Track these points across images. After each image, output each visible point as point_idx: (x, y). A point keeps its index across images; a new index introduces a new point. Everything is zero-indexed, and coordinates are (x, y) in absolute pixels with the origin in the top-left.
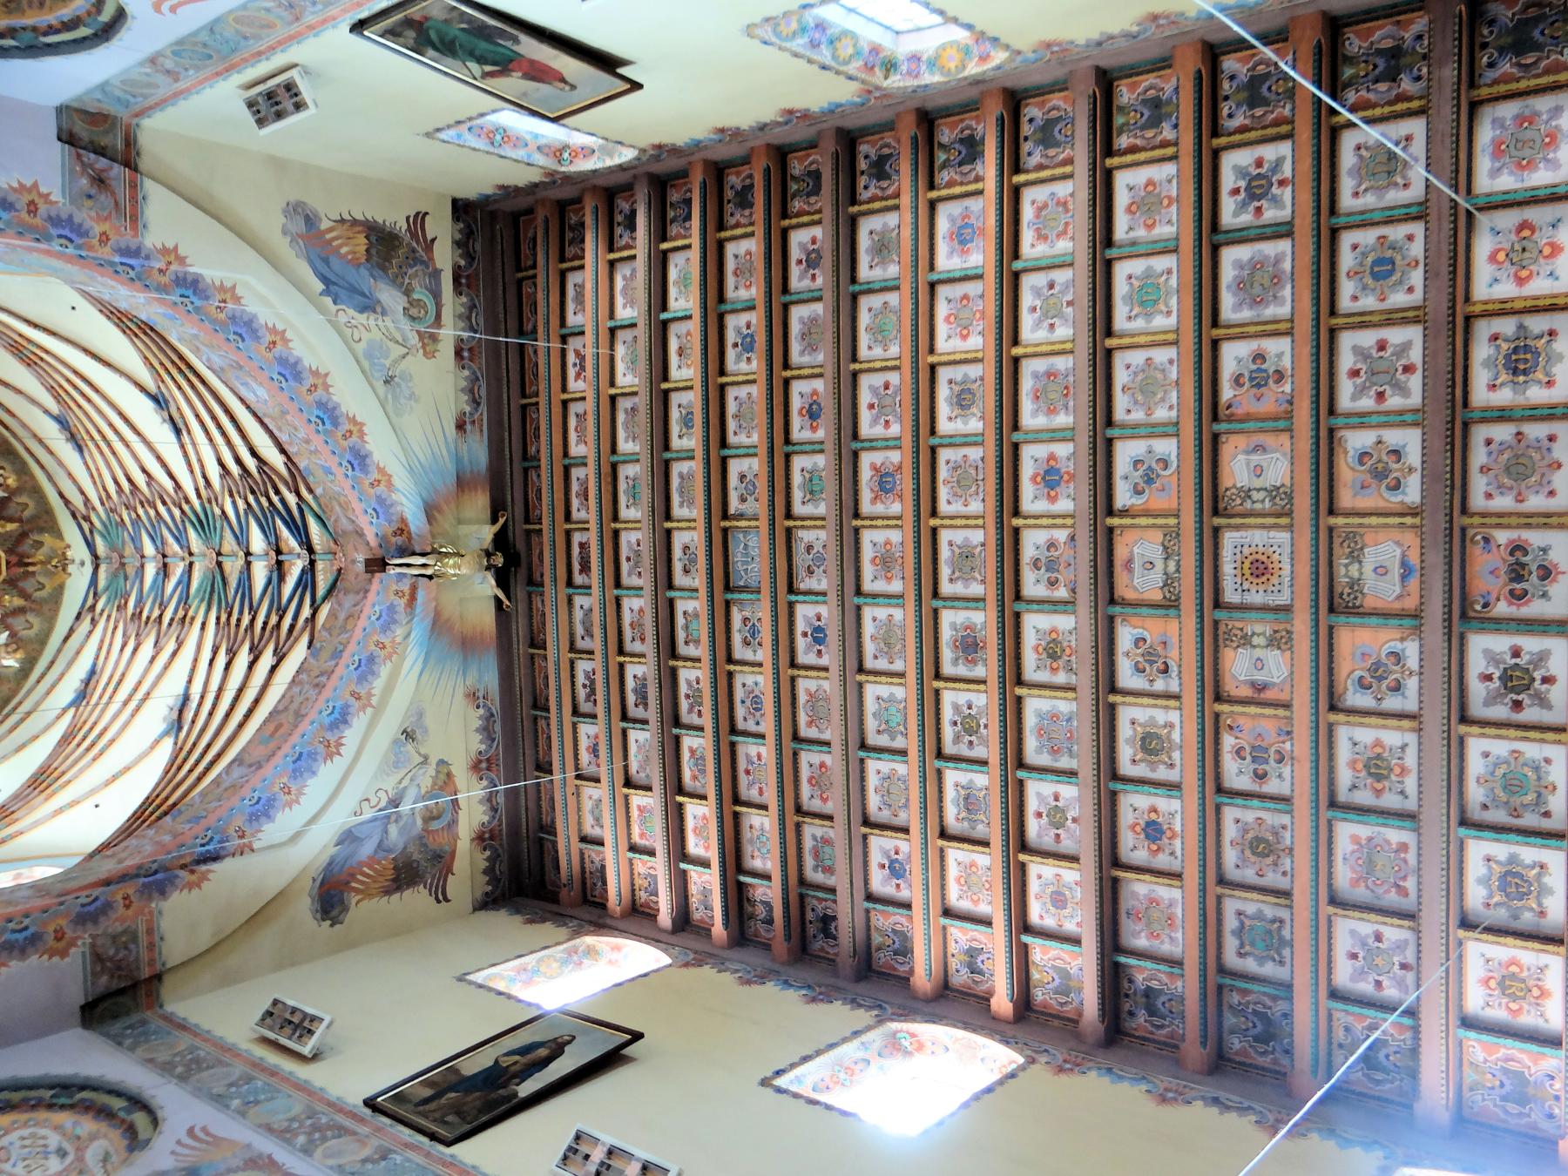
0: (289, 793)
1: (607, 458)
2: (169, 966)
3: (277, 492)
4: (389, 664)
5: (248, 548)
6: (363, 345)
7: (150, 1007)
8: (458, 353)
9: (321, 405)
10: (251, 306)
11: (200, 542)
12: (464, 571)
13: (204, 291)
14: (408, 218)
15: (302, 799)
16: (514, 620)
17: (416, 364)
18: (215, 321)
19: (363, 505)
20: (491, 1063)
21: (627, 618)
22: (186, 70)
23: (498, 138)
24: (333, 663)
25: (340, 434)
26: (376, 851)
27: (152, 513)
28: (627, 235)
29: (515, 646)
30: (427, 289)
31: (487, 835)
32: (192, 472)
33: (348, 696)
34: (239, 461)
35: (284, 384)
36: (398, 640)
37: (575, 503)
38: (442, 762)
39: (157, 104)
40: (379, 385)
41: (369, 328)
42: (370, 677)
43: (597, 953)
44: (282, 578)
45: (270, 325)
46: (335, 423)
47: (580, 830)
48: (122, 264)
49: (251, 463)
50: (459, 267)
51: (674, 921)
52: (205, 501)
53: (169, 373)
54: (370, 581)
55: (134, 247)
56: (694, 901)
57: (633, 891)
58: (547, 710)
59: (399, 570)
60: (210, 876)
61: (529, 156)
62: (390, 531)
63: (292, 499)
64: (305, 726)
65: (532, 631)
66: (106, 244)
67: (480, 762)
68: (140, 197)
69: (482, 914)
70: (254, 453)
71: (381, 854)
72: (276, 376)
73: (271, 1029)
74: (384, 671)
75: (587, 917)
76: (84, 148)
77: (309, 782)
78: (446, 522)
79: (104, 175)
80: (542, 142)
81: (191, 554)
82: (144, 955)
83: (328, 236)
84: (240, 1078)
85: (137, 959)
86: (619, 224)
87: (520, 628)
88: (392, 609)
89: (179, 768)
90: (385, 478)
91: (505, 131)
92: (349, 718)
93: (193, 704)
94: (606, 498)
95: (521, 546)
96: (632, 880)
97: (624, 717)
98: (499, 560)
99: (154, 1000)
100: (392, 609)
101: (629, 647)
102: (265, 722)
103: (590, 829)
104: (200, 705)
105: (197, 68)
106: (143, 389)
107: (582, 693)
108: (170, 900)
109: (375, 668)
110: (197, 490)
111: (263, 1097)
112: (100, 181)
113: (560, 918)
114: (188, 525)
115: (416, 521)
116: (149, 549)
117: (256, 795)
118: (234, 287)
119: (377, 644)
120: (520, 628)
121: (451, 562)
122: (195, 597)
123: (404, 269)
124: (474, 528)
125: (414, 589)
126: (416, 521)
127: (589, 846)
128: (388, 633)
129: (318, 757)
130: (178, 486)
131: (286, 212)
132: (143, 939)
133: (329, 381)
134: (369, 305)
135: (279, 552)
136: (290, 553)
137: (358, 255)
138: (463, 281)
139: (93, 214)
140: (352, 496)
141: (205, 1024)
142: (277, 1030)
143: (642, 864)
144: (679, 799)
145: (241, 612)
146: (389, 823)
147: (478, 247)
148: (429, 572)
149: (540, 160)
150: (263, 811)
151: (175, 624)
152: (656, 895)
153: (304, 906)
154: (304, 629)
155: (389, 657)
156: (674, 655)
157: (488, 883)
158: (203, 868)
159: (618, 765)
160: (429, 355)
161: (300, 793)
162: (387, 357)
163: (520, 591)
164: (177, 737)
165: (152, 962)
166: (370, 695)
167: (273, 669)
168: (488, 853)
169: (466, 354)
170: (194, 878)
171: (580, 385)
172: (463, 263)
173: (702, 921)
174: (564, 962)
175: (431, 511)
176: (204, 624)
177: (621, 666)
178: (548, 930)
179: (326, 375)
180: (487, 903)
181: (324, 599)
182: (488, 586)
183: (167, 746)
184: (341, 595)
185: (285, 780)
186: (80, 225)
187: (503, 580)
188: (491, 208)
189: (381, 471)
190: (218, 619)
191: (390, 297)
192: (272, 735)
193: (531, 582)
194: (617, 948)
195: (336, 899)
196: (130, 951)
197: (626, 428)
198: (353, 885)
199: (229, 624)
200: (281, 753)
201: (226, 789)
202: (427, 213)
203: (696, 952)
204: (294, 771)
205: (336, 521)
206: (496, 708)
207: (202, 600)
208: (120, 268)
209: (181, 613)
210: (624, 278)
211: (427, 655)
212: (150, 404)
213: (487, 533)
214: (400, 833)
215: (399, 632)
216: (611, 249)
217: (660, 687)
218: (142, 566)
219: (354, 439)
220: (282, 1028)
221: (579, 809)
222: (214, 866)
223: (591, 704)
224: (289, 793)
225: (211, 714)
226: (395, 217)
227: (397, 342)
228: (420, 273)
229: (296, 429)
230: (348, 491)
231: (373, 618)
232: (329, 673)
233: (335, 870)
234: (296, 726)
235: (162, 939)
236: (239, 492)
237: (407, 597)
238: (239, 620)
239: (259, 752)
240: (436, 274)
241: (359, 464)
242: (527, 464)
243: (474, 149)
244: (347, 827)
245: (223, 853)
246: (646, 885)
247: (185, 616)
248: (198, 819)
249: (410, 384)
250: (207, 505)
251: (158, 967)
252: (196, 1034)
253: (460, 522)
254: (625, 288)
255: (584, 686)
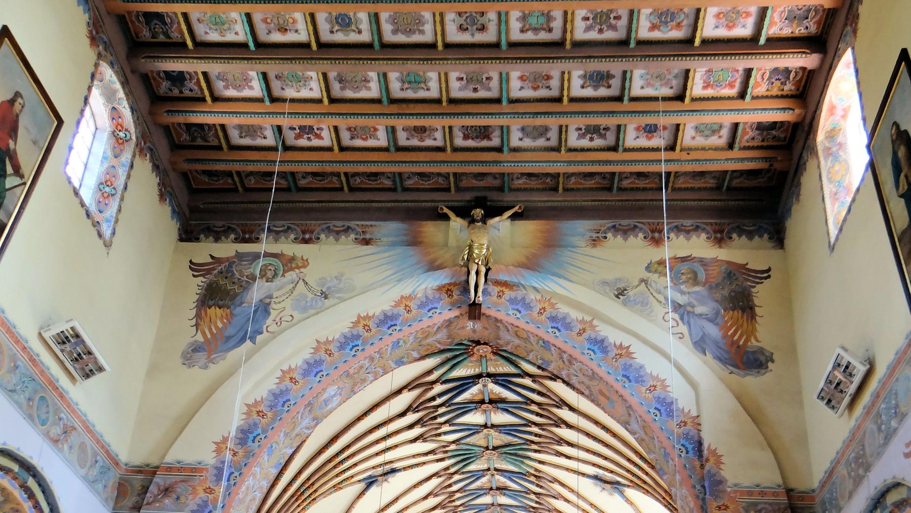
0: (655, 387)
1: (386, 108)
2: (779, 481)
3: (433, 399)
4: (558, 306)
5: (481, 426)
6: (295, 314)
7: (813, 499)
8: (306, 241)
9: (342, 347)
10: (262, 393)
11: (477, 461)
12: (485, 242)
13: (250, 425)
14: (194, 276)
15: (662, 377)
16: (532, 204)
17: (312, 274)
18: (273, 420)
19: (425, 319)
20: (902, 200)
21: (528, 93)
22: (60, 419)
23: (107, 189)
24: (553, 348)
25: (366, 334)
26: (716, 324)
27: (458, 495)
28: (192, 85)
29: (556, 204)
30: (251, 264)
31: (719, 235)
32: (424, 463)
33: (581, 338)
34: (411, 427)
35: (325, 373)
36: (539, 297)
37: (429, 143)
38: (648, 268)
39: (98, 442)
40: (327, 302)
41: (282, 308)
42: (568, 321)
43: (833, 130)
44: (503, 401)
45: (277, 381)
46: (358, 337)
47: (722, 149)
48: (228, 480)
49: (411, 418)
50: (235, 239)
51: (813, 52)
52: (446, 455)
53: (344, 471)
54: (488, 317)
55: (215, 472)
56: (799, 30)
57: (782, 97)
58: (613, 174)
59: (480, 293)
60: (713, 447)
61: (124, 165)
62: (447, 299)
63: (438, 388)
64: (602, 372)
65: (544, 190)
66: (213, 490)
67: (653, 238)
68: (178, 465)
69: (787, 242)
70: (403, 414)
71: (719, 320)
72: (318, 379)
73: (839, 403)
74: (563, 309)
75: (801, 143)
76: (143, 500)
77: (648, 371)
78: (444, 256)
79: (162, 488)
80: (109, 153)
81: (489, 469)
82: (769, 499)
83: (209, 336)
84: (876, 422)
85: (770, 504)
86: (181, 92)
87: (541, 199)
88: (512, 301)
89: (645, 482)
90: (404, 300)
91: (102, 184)
92: (599, 338)
93: (601, 472)
94: (419, 109)
95: (468, 196)
96: (772, 97)
97: (619, 99)
98: (478, 212)
99: (808, 495)
100: (512, 301)
101: (555, 93)
102: (598, 405)
103: (721, 140)
104: (600, 467)
105: (57, 411)
106: (362, 493)
107: (598, 142)
108: (727, 478)
109: (560, 316)
110: (438, 460)
111: (893, 402)
112: (167, 491)
113: (798, 168)
114: (465, 470)
115: (441, 278)
116: (487, 499)
117: (652, 411)
118: (247, 405)
119: (540, 313)
120: (541, 199)
121: (476, 251)
122: (520, 467)
123: (236, 280)
124: (451, 234)
125: (497, 283)
126: (441, 278)
127: (738, 140)
128: (532, 305)
129: (628, 363)
130: (436, 475)
131: (190, 366)
132: (755, 499)
133: (323, 340)
134: (264, 308)
135: (482, 402)
136: (482, 393)
137: (224, 315)
138: (247, 236)
139: (190, 497)
140: (417, 326)
141: (832, 455)
142: (844, 395)
143: (759, 86)
144: (697, 42)
145: (530, 433)
146: (693, 313)
147: (220, 223)
148: (483, 270)
149: (126, 157)
150: (666, 406)
151: (541, 484)
152: (787, 71)
153: (752, 382)
154: (542, 384)
155: (553, 305)
156: (560, 44)
157: (761, 236)
158: (705, 452)
159: (661, 106)
160: (305, 263)
161: (657, 378)
162: (307, 297)
163: (508, 197)
164: (624, 485)
165: (775, 494)
166: (583, 321)
167: (572, 409)
168: (734, 236)
169: (307, 236)
170: (712, 460)
171: (325, 134)
172: (232, 236)
173: (818, 23)
174: (836, 158)
175: (433, 267)
176: (541, 462)
177: (572, 100)
178: (807, 180)
179: (318, 342)
180: (778, 238)
181: (516, 366)
182: (501, 225)
183: (631, 493)
184: (501, 342)
185: (644, 389)
186: (199, 505)
187: (493, 211)
188: (187, 213)
189: (398, 304)
190: (536, 451)
191: (257, 292)
192: (608, 398)
193: (501, 189)
194: (832, 108)
195: (751, 357)
196: (764, 508)
197: (357, 89)
198: (741, 343)
199: (539, 443)
200: (622, 391)
201: (646, 434)
202: (191, 262)
203: (846, 25)
204: (637, 382)
205: (440, 343)
206: (608, 223)
207: (523, 462)
208: (232, 482)
209: (532, 479)
210: (226, 87)
211: (554, 274)
212: (374, 489)
213: (457, 223)
214: (702, 303)
215: (532, 296)
216: (203, 100)
217: (590, 57)
218: (500, 505)
219: (371, 324)
220: (841, 391)
221: (703, 149)
222: (706, 445)
223: (608, 133)
224: (655, 387)
225: (606, 458)
226: (194, 286)
227: (294, 288)
228: (238, 268)
229: (361, 367)
230: (412, 330)
231: (519, 315)
232: (561, 351)
233: (726, 356)
234: (601, 378)
235: (758, 486)
236: (437, 429)
237: (504, 289)
238: (536, 435)
239: (621, 410)
240: (240, 256)
241: (392, 320)
242: (399, 189)
243: (119, 210)
244: (691, 346)
245: (696, 438)
246: (778, 83)
247: (536, 476)
248: (666, 455)
249: (329, 279)
250: (450, 454)
251: (781, 490)
252: (838, 462)
253: (446, 245)
254: (235, 87)
255: (591, 139)
